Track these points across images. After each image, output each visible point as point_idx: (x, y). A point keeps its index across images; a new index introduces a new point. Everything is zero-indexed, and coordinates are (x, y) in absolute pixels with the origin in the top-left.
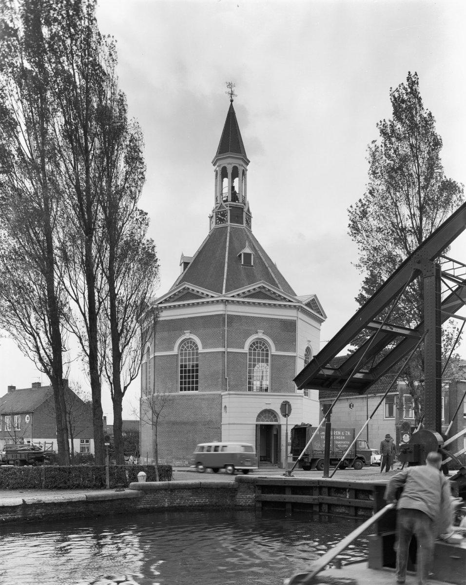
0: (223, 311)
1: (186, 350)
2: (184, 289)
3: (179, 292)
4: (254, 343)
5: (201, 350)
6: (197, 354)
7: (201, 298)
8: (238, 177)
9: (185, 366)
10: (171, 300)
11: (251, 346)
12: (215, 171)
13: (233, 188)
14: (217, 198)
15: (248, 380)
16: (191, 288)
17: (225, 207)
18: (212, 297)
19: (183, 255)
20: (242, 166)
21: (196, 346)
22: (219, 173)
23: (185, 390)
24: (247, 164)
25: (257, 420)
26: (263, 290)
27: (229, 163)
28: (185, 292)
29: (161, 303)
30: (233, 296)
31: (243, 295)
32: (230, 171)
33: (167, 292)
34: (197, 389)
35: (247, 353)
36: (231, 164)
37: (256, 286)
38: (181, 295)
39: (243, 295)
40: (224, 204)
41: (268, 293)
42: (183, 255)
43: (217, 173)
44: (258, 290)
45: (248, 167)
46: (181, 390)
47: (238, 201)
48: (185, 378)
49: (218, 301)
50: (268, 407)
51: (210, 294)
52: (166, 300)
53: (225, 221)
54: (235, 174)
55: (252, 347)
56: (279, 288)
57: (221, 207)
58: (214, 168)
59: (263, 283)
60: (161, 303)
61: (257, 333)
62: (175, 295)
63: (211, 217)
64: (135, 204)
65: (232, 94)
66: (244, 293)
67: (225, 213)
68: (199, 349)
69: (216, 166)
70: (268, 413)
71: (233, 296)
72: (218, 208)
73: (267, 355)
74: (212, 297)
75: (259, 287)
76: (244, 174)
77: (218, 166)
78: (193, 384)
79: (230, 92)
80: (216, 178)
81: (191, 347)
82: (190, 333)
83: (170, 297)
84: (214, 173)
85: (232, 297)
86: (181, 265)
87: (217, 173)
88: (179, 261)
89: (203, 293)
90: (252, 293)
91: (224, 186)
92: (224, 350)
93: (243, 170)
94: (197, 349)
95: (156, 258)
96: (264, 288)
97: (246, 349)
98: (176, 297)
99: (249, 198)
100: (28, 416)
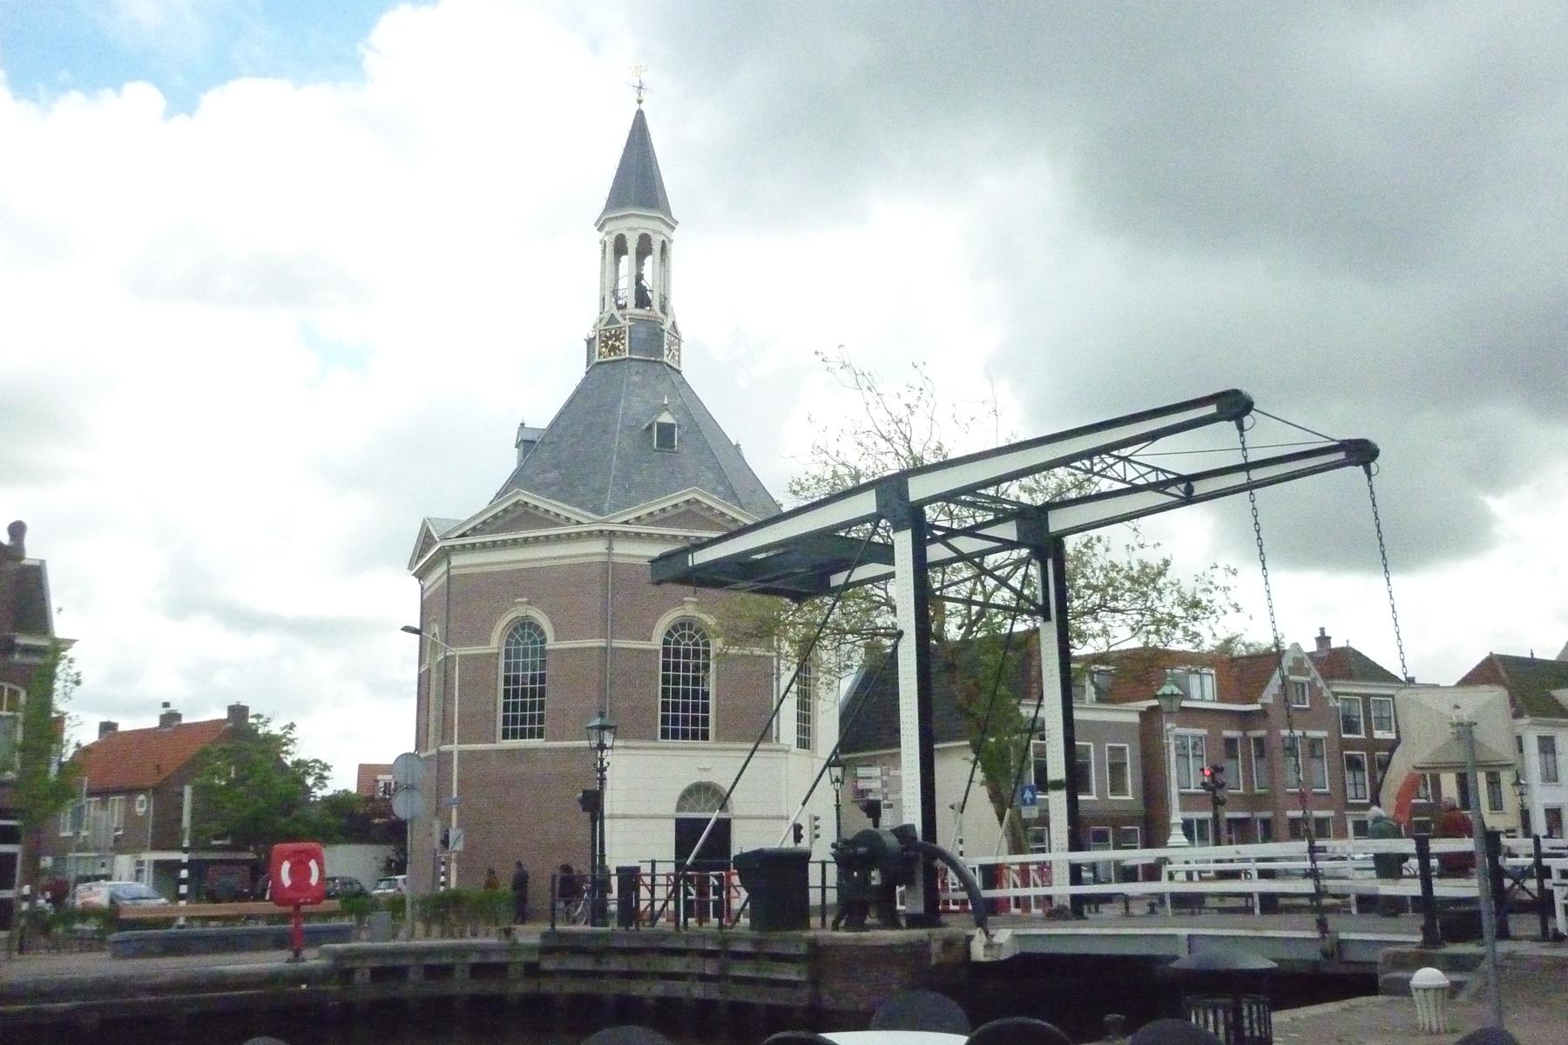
0: (604, 554)
1: (517, 643)
2: (516, 504)
3: (505, 511)
4: (675, 628)
5: (551, 644)
6: (544, 652)
7: (556, 525)
8: (651, 254)
9: (516, 682)
10: (488, 528)
11: (669, 634)
12: (601, 243)
13: (639, 278)
14: (604, 299)
15: (661, 673)
16: (532, 502)
17: (620, 319)
18: (579, 523)
19: (522, 424)
20: (660, 233)
21: (542, 633)
22: (610, 249)
23: (514, 737)
24: (673, 228)
25: (679, 808)
26: (695, 508)
27: (632, 227)
28: (520, 510)
29: (463, 535)
30: (626, 522)
31: (649, 520)
32: (632, 245)
33: (485, 506)
34: (540, 735)
35: (657, 651)
36: (635, 229)
37: (679, 497)
38: (509, 517)
39: (649, 520)
40: (618, 314)
41: (707, 514)
42: (522, 424)
43: (605, 247)
44: (684, 508)
45: (674, 235)
46: (505, 736)
47: (651, 306)
48: (515, 710)
49: (590, 533)
50: (704, 778)
51: (574, 518)
52: (474, 529)
53: (620, 350)
54: (644, 248)
55: (672, 636)
56: (556, 521)
57: (612, 320)
58: (600, 235)
59: (695, 491)
60: (463, 535)
61: (683, 603)
62: (495, 517)
63: (590, 342)
64: (1215, 911)
65: (640, 88)
66: (651, 514)
67: (620, 334)
68: (548, 642)
69: (603, 233)
70: (701, 792)
71: (626, 522)
72: (604, 322)
73: (707, 653)
74: (579, 523)
75: (688, 501)
76: (664, 249)
77: (607, 233)
78: (532, 722)
79: (638, 84)
80: (604, 258)
81: (530, 635)
82: (529, 603)
83: (484, 523)
84: (600, 247)
85: (457, 537)
86: (517, 446)
87: (605, 247)
88: (512, 437)
89: (558, 515)
90: (682, 509)
91: (620, 275)
92: (603, 644)
93: (663, 241)
94: (544, 641)
95: (1414, 771)
96: (698, 501)
97: (657, 643)
98: (500, 523)
99: (675, 302)
100: (142, 797)
